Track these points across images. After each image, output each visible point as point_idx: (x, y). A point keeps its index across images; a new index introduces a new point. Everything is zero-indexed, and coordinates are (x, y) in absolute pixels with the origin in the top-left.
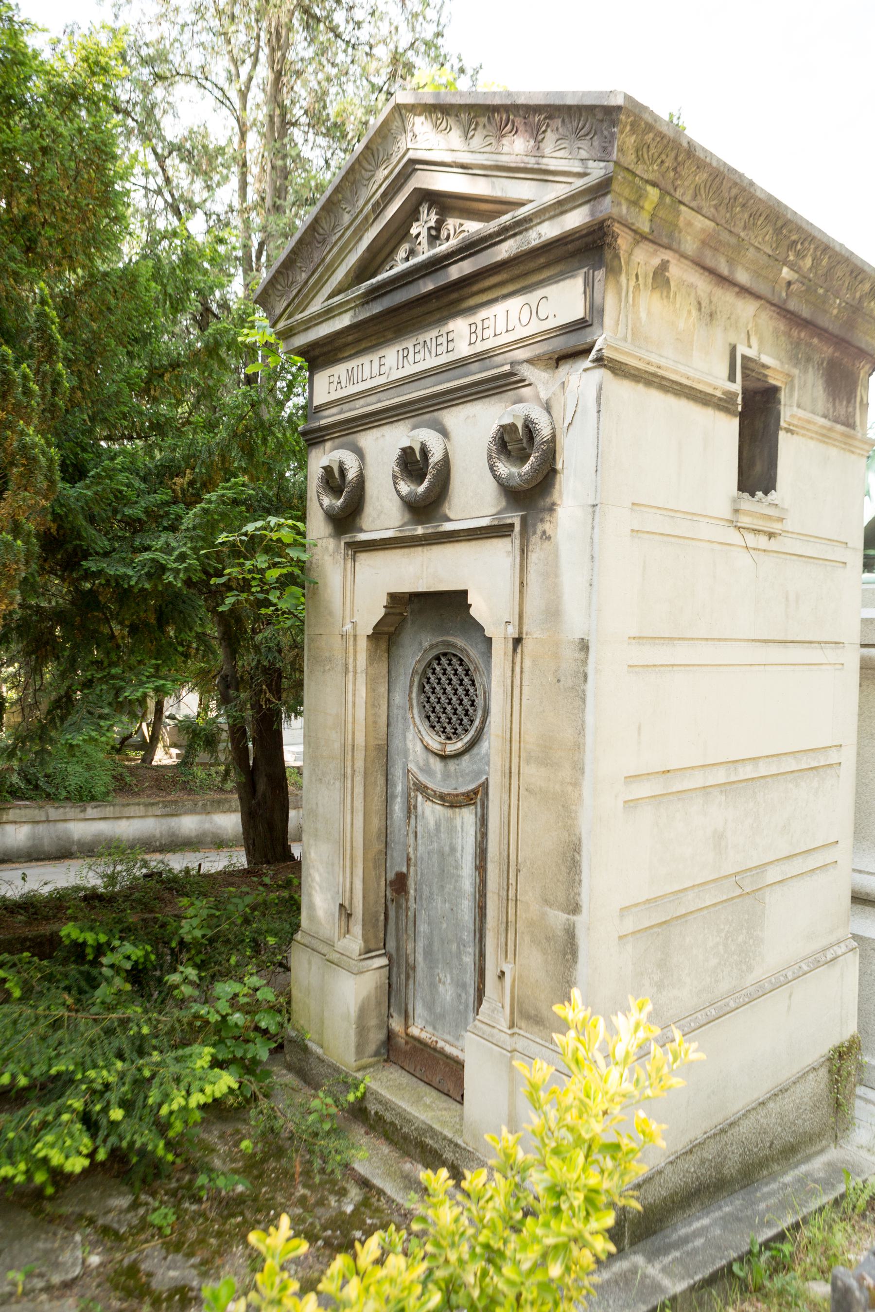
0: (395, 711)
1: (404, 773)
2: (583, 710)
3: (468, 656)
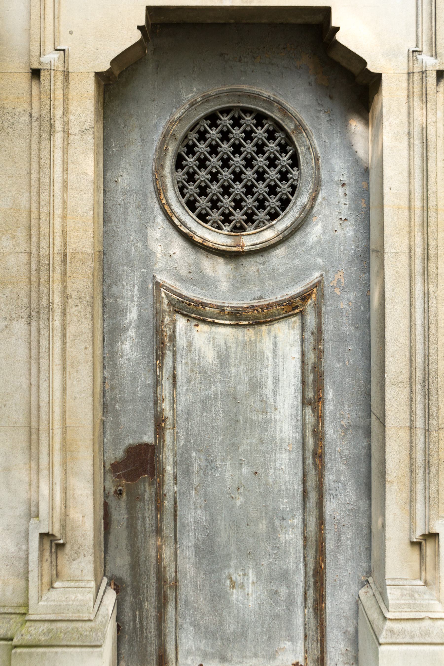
0: (120, 198)
1: (143, 291)
3: (283, 110)
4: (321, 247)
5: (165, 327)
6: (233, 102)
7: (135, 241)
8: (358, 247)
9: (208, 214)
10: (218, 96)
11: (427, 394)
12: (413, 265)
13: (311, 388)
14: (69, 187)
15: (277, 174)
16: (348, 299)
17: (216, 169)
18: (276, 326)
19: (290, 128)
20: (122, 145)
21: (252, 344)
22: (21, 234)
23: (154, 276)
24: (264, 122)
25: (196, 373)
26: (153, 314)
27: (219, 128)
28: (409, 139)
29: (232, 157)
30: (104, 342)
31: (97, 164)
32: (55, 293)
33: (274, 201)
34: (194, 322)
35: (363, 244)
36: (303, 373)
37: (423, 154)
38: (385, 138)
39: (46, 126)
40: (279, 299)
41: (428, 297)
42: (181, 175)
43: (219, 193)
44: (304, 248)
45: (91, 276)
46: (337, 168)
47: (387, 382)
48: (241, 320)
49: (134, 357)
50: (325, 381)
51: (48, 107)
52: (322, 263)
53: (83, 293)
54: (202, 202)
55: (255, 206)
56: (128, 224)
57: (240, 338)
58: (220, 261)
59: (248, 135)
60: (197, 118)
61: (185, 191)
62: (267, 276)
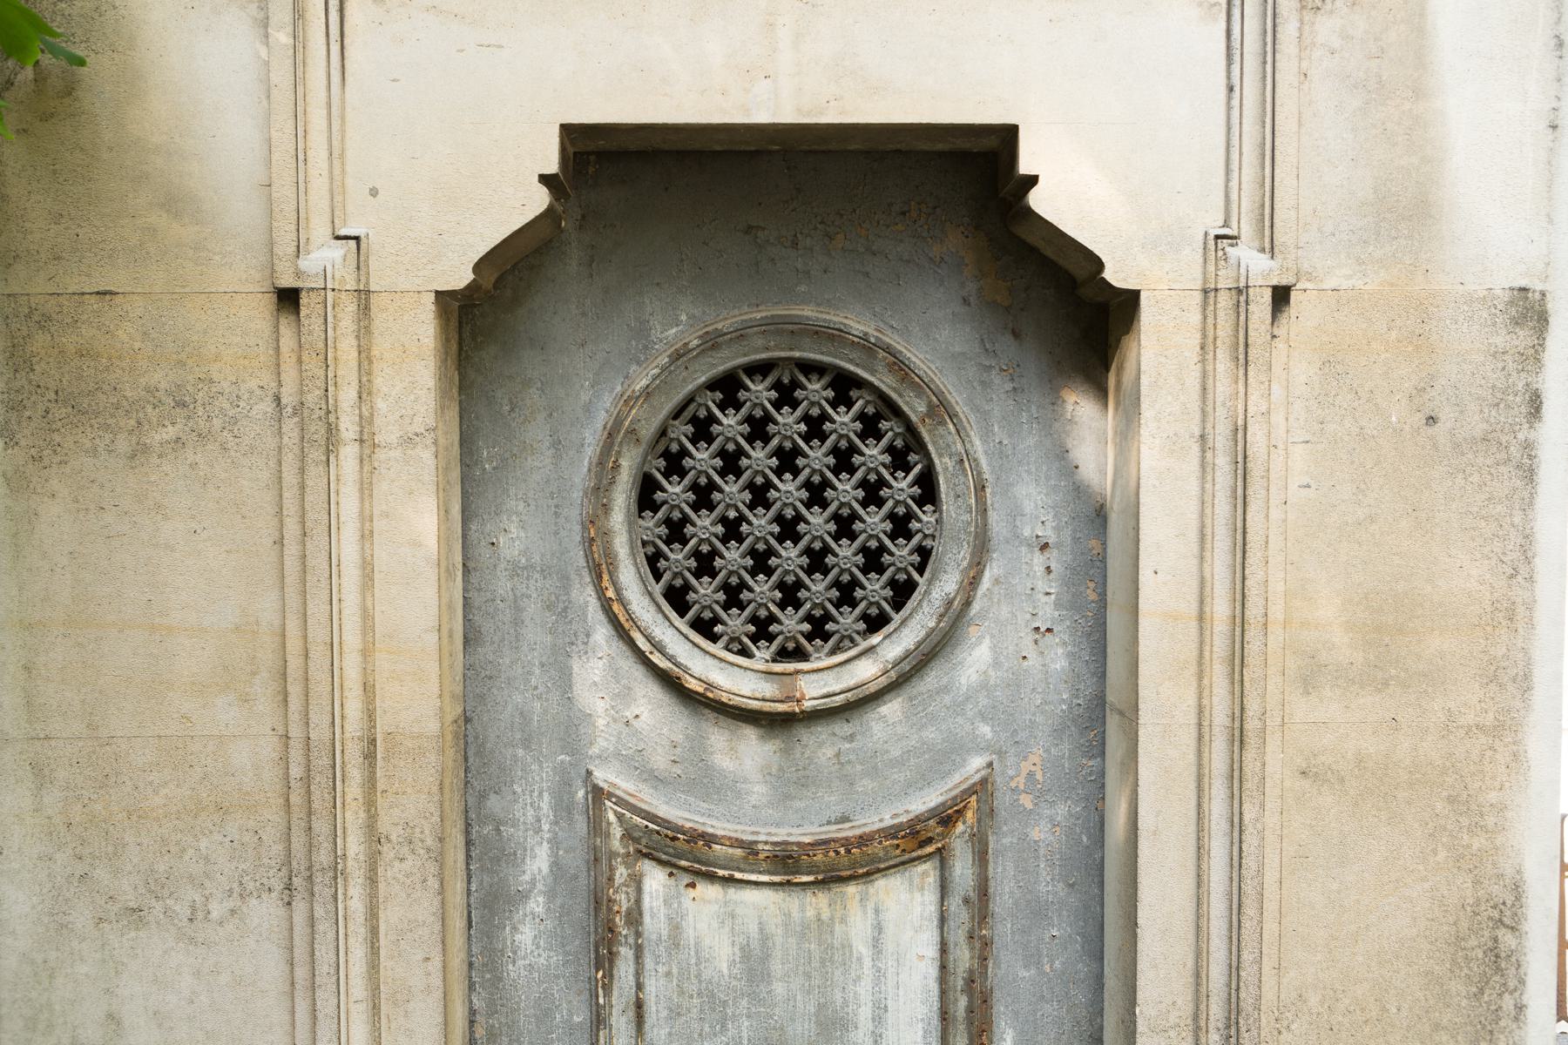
0: (503, 585)
1: (563, 808)
2: (1529, 504)
3: (900, 367)
4: (988, 696)
5: (616, 892)
6: (777, 347)
7: (541, 689)
8: (1077, 697)
9: (716, 620)
10: (740, 335)
11: (1236, 797)
12: (1206, 755)
13: (962, 1027)
14: (377, 576)
15: (883, 520)
16: (1051, 820)
17: (737, 510)
18: (881, 883)
19: (915, 411)
20: (507, 455)
21: (823, 927)
22: (263, 690)
23: (589, 773)
24: (854, 394)
25: (691, 997)
26: (588, 862)
27: (744, 411)
28: (1204, 451)
29: (776, 481)
30: (470, 926)
31: (445, 511)
32: (349, 832)
33: (877, 587)
34: (687, 879)
35: (1088, 688)
36: (943, 993)
37: (1235, 491)
38: (1143, 448)
39: (317, 430)
40: (888, 822)
41: (1241, 831)
42: (651, 525)
43: (745, 568)
44: (947, 699)
45: (435, 789)
46: (1029, 505)
47: (1141, 1026)
48: (798, 872)
49: (542, 960)
50: (994, 1011)
51: (320, 383)
52: (989, 736)
53: (418, 830)
54: (703, 592)
55: (830, 600)
56: (525, 648)
57: (796, 915)
58: (750, 733)
59: (815, 428)
60: (690, 387)
61: (662, 564)
62: (859, 768)
